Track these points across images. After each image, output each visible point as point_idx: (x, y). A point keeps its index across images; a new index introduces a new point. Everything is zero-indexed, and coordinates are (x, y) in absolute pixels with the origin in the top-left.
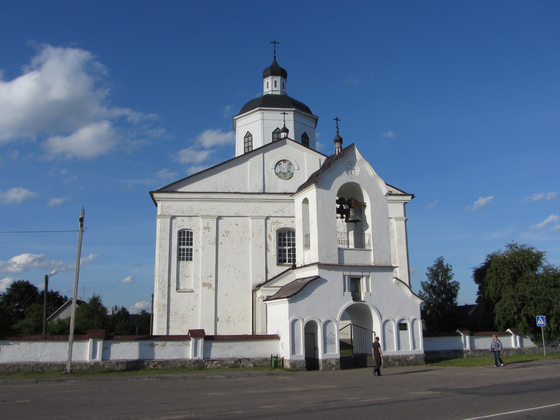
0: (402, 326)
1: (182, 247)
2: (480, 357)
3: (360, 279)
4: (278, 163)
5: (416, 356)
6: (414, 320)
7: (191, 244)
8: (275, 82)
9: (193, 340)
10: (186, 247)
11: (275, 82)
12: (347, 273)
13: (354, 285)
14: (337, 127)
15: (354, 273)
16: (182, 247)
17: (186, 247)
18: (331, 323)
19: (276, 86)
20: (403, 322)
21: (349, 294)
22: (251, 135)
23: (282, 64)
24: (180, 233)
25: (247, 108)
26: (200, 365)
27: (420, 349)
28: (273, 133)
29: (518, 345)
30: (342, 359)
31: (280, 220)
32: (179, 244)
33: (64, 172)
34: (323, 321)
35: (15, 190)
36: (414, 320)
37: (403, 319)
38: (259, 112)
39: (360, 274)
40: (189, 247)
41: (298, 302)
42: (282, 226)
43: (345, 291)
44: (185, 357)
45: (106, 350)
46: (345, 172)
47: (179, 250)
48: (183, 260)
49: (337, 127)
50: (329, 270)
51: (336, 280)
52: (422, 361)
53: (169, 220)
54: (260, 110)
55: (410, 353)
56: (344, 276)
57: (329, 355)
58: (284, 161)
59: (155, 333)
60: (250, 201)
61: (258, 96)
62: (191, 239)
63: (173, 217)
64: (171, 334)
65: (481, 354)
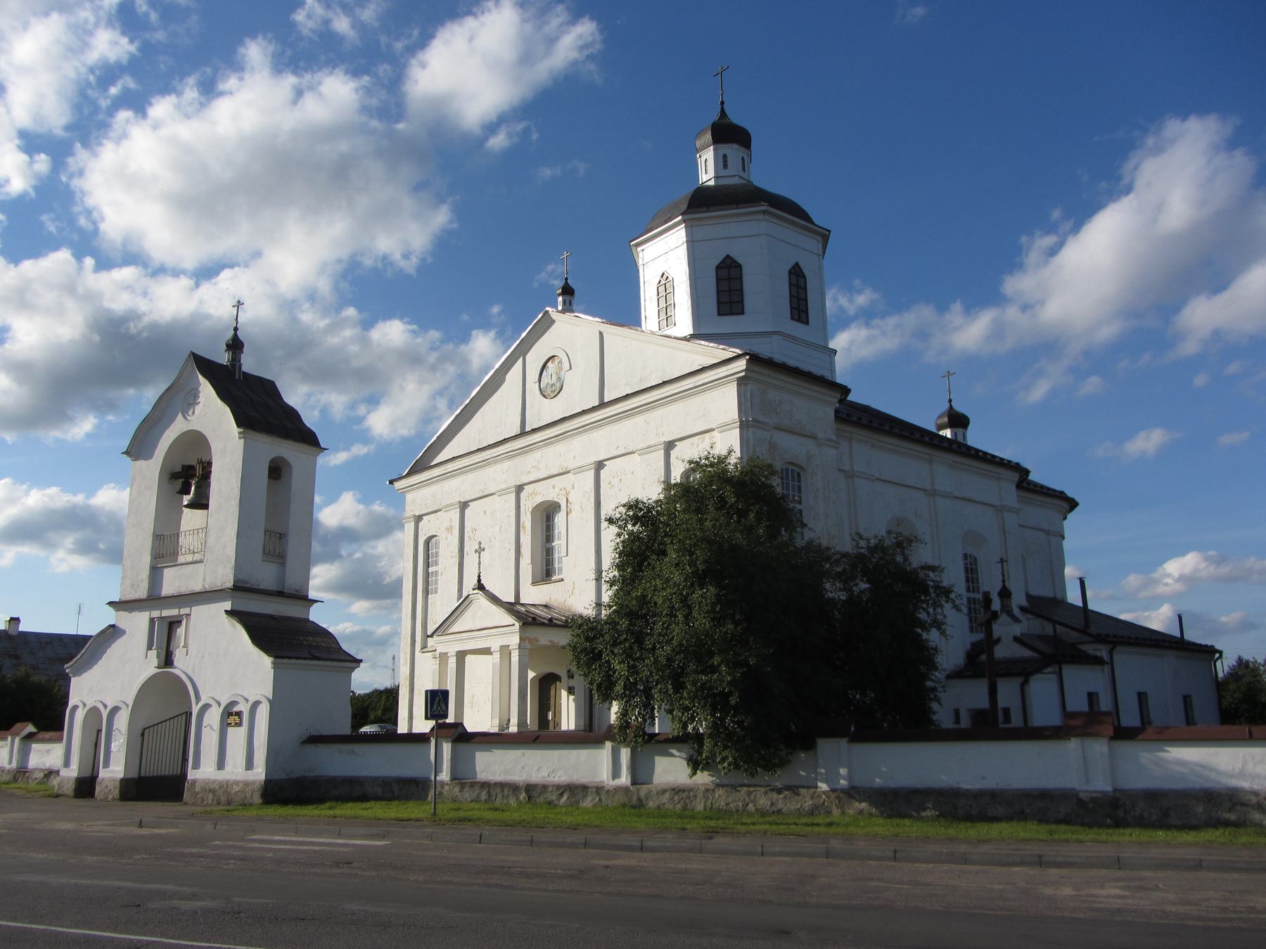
0: (230, 715)
2: (477, 800)
5: (246, 784)
6: (257, 704)
8: (725, 157)
11: (725, 157)
12: (156, 614)
13: (165, 638)
15: (166, 613)
19: (725, 166)
20: (236, 709)
21: (153, 659)
23: (735, 117)
27: (259, 773)
28: (718, 268)
29: (624, 779)
30: (268, 782)
33: (1233, 368)
34: (252, 699)
35: (1142, 434)
36: (257, 704)
38: (761, 217)
41: (84, 675)
43: (150, 647)
45: (25, 754)
46: (180, 416)
50: (131, 610)
52: (257, 799)
54: (764, 212)
55: (239, 778)
56: (152, 621)
59: (402, 728)
60: (486, 463)
64: (415, 731)
65: (484, 796)
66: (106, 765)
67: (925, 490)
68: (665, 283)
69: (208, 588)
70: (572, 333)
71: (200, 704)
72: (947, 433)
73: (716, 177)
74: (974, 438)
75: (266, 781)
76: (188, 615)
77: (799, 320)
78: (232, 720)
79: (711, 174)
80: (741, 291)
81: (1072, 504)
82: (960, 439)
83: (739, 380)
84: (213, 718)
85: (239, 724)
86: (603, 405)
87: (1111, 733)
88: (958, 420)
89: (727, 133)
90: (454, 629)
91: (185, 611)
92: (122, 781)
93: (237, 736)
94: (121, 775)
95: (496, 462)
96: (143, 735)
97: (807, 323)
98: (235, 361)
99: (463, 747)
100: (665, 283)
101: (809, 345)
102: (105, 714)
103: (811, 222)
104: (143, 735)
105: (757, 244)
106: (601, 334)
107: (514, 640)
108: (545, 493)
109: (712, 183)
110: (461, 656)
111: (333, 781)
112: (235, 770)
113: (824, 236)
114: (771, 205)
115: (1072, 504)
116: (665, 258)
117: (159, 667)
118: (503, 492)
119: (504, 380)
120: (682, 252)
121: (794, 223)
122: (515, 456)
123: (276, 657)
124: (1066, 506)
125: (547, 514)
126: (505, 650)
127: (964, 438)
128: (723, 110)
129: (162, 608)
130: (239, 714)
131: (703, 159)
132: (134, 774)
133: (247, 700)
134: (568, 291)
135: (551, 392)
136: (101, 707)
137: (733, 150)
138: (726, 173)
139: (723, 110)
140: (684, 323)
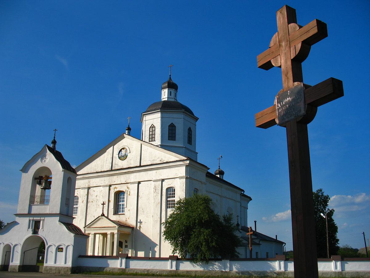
1: (169, 199)
3: (40, 221)
4: (121, 151)
5: (65, 268)
7: (174, 197)
8: (171, 92)
9: (170, 261)
10: (171, 199)
11: (171, 92)
12: (31, 218)
13: (36, 226)
14: (55, 135)
15: (35, 218)
16: (169, 199)
17: (171, 199)
18: (18, 246)
19: (171, 95)
20: (60, 247)
22: (155, 127)
23: (174, 81)
24: (167, 189)
25: (150, 110)
26: (122, 272)
27: (69, 264)
28: (169, 126)
31: (117, 186)
32: (167, 197)
34: (66, 245)
37: (60, 245)
38: (182, 113)
39: (39, 218)
40: (173, 199)
42: (118, 190)
43: (29, 228)
44: (166, 269)
47: (167, 201)
48: (170, 208)
49: (55, 135)
50: (20, 217)
51: (24, 222)
53: (161, 182)
56: (30, 220)
57: (67, 265)
58: (123, 148)
61: (157, 101)
62: (174, 194)
63: (163, 180)
66: (12, 261)
67: (220, 195)
68: (153, 127)
69: (51, 213)
70: (128, 141)
71: (48, 246)
72: (218, 176)
73: (168, 98)
74: (225, 178)
75: (72, 267)
76: (43, 220)
77: (189, 144)
78: (59, 250)
79: (166, 96)
80: (175, 133)
81: (251, 199)
82: (221, 178)
83: (186, 165)
84: (53, 249)
85: (62, 251)
86: (140, 166)
87: (285, 259)
88: (221, 173)
89: (172, 86)
90: (95, 226)
91: (43, 218)
92: (19, 266)
93: (61, 255)
94: (19, 264)
95: (102, 177)
96: (24, 253)
97: (191, 144)
98: (54, 147)
99: (128, 260)
100: (153, 127)
101: (191, 151)
102: (12, 247)
103: (193, 114)
104: (24, 253)
105: (179, 120)
106: (141, 144)
107: (116, 232)
108: (120, 188)
109: (166, 99)
110: (95, 234)
111: (89, 268)
112: (61, 263)
113: (197, 119)
114: (185, 110)
115: (251, 199)
116: (153, 121)
117: (32, 234)
118: (106, 186)
119: (106, 152)
120: (159, 120)
121: (189, 115)
122: (110, 176)
123: (75, 234)
124: (249, 199)
125: (119, 195)
126: (113, 234)
127: (223, 178)
128: (170, 78)
129: (34, 217)
130: (62, 249)
131: (164, 91)
132: (22, 265)
133: (4, 244)
134: (129, 129)
135: (123, 158)
136: (11, 244)
137: (173, 91)
138: (170, 97)
139: (170, 78)
140: (158, 141)
